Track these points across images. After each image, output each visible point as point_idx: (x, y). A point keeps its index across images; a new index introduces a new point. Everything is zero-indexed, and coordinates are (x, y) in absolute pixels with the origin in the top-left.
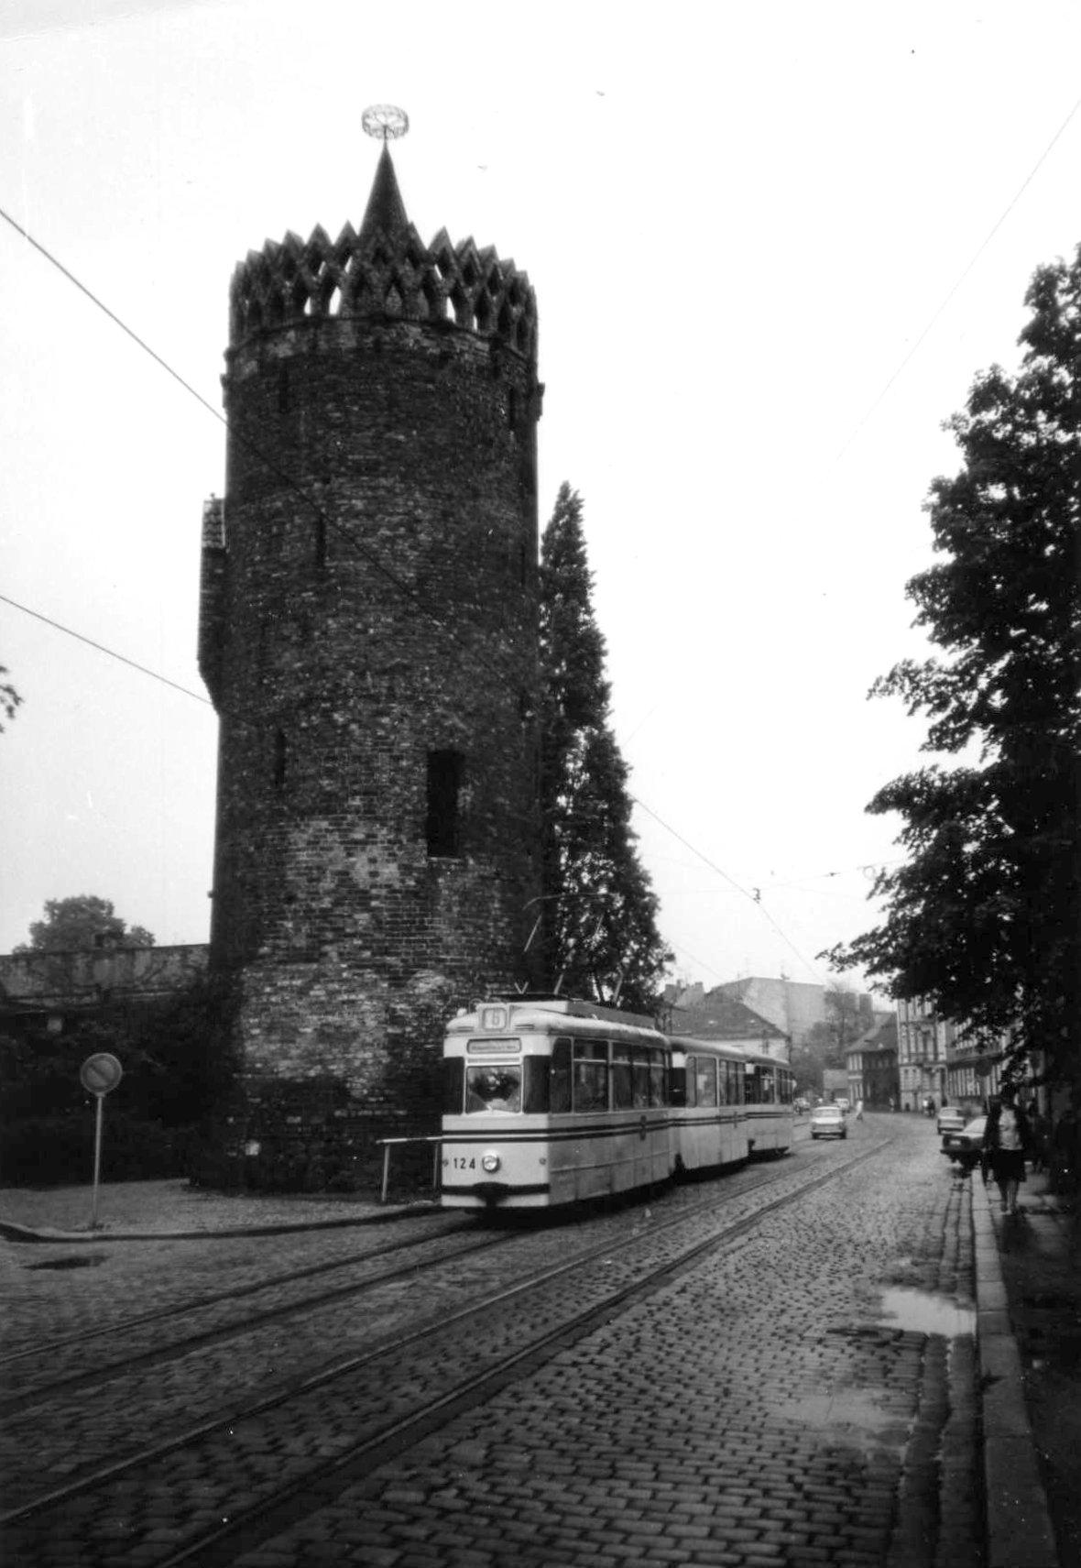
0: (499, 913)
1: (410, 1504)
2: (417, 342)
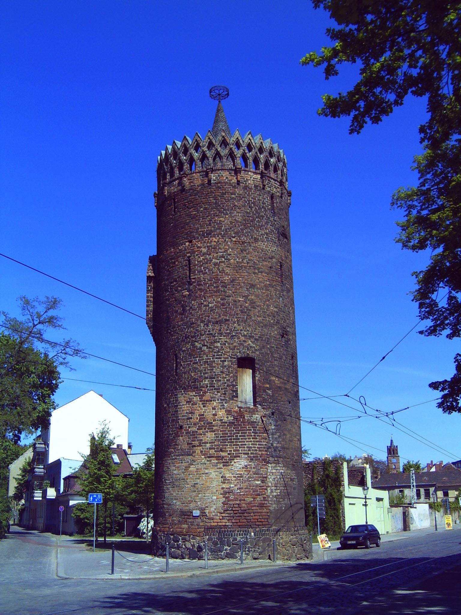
2: (227, 178)
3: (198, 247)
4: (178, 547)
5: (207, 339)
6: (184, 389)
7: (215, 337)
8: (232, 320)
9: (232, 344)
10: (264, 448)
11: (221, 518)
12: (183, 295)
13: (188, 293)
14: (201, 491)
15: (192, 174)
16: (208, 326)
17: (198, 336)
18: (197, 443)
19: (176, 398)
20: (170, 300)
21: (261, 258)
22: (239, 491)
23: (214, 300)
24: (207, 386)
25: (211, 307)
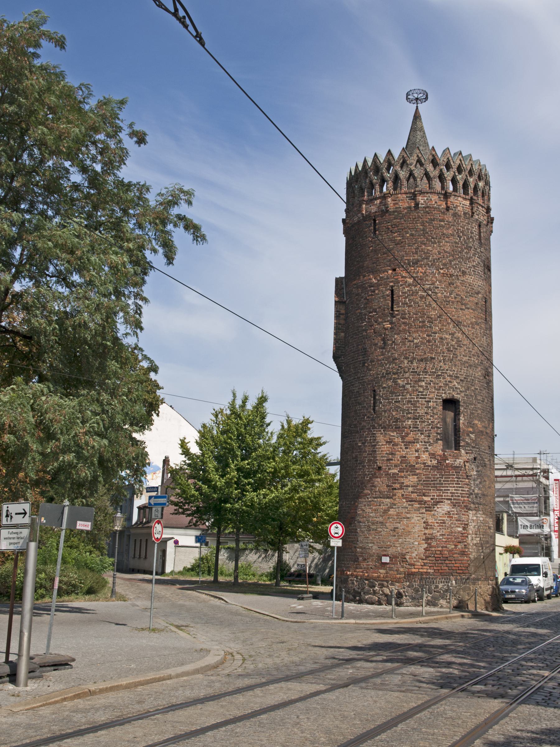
0: (476, 477)
1: (447, 653)
2: (436, 202)
3: (403, 277)
4: (375, 593)
5: (411, 377)
6: (384, 428)
7: (420, 375)
8: (438, 358)
9: (438, 384)
10: (466, 494)
11: (423, 564)
12: (384, 328)
13: (390, 326)
14: (401, 536)
15: (397, 194)
16: (412, 363)
17: (400, 373)
18: (397, 486)
19: (374, 437)
20: (368, 331)
21: (468, 293)
22: (441, 537)
23: (419, 336)
24: (410, 427)
25: (416, 344)
